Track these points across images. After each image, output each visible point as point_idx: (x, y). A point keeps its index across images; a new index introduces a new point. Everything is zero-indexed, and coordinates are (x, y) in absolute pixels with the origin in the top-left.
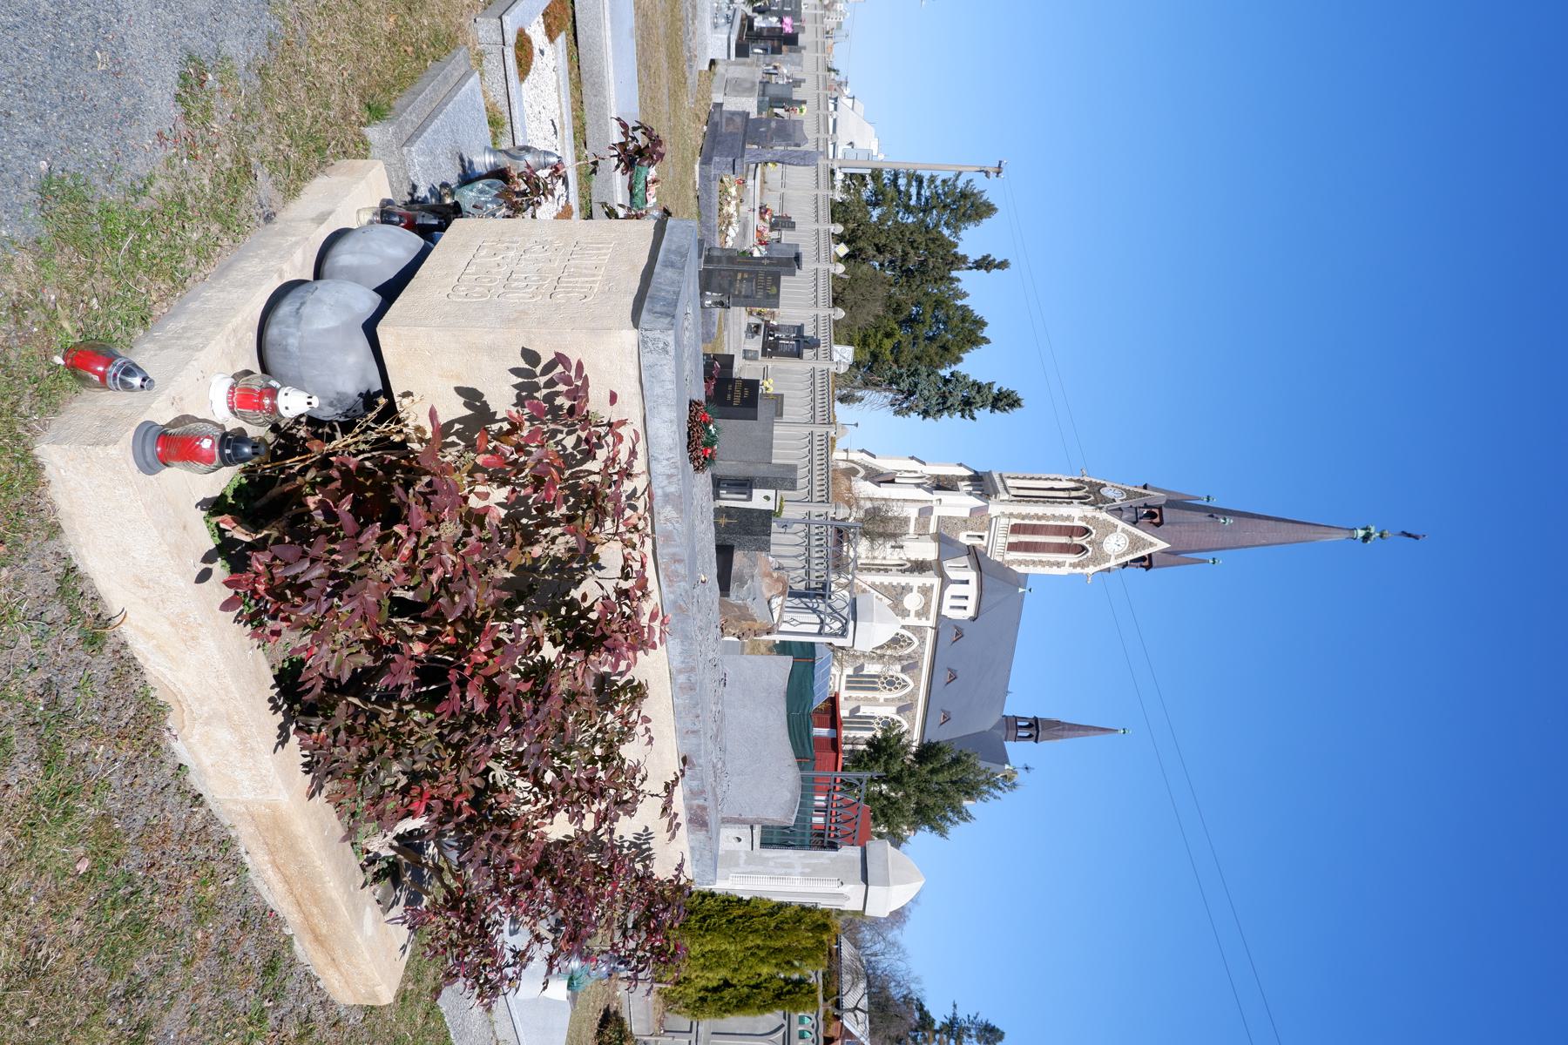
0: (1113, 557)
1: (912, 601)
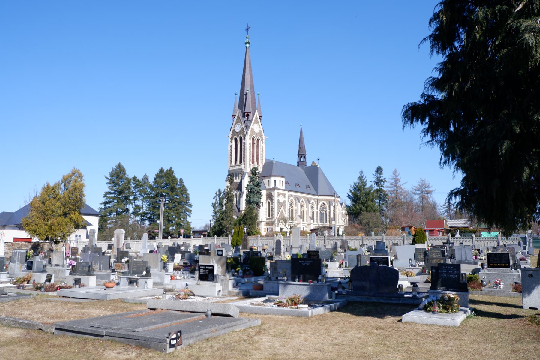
1: (282, 199)
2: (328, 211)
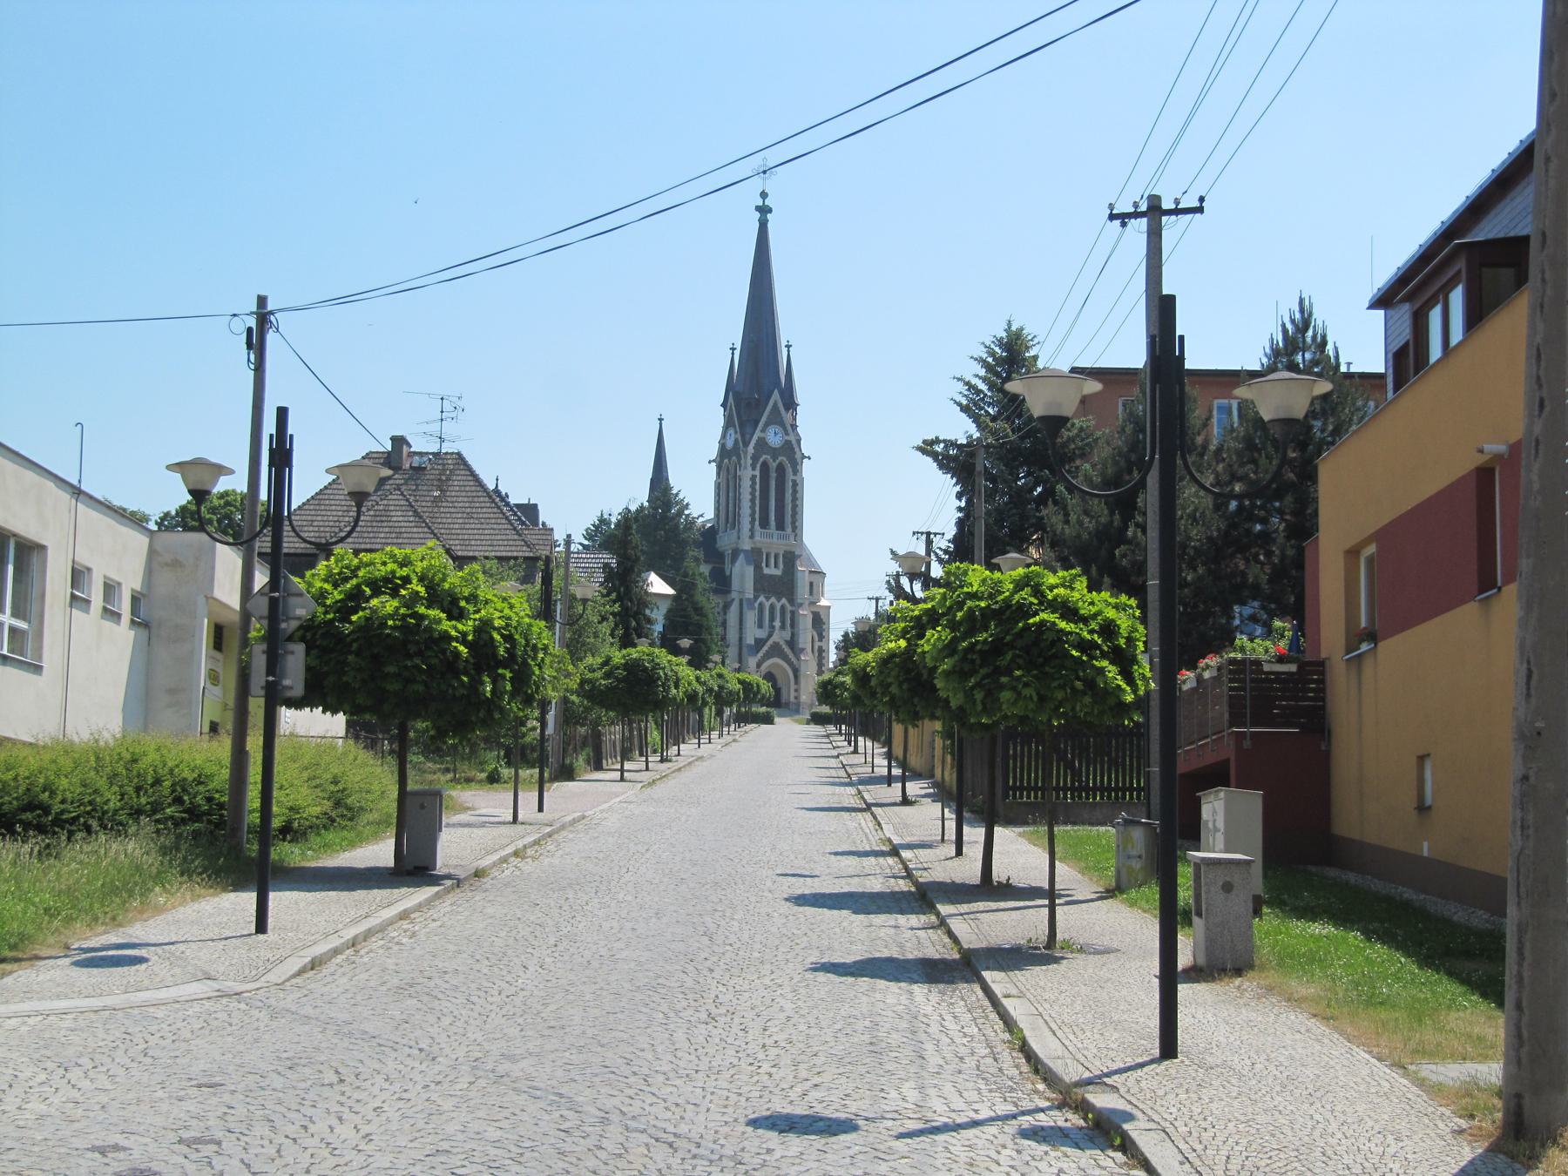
0: (787, 438)
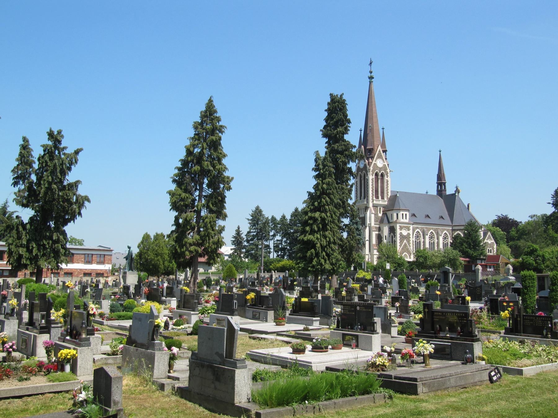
1: (405, 233)
2: (436, 241)
